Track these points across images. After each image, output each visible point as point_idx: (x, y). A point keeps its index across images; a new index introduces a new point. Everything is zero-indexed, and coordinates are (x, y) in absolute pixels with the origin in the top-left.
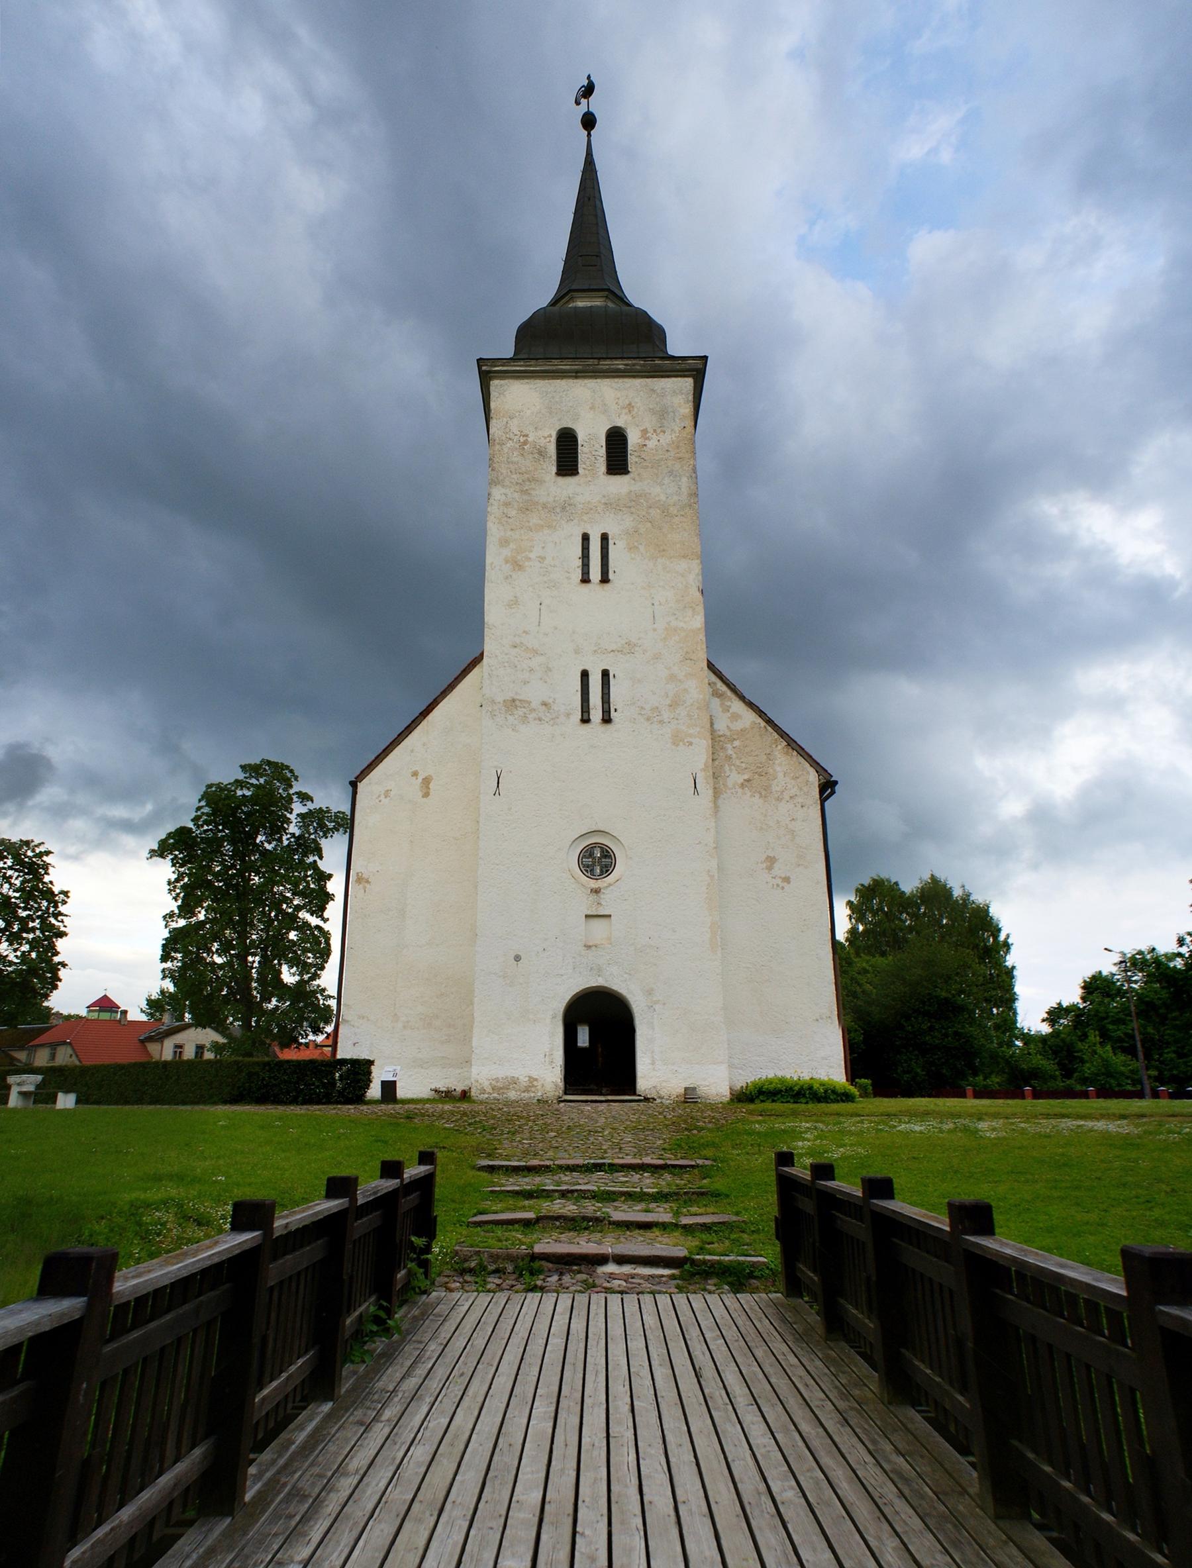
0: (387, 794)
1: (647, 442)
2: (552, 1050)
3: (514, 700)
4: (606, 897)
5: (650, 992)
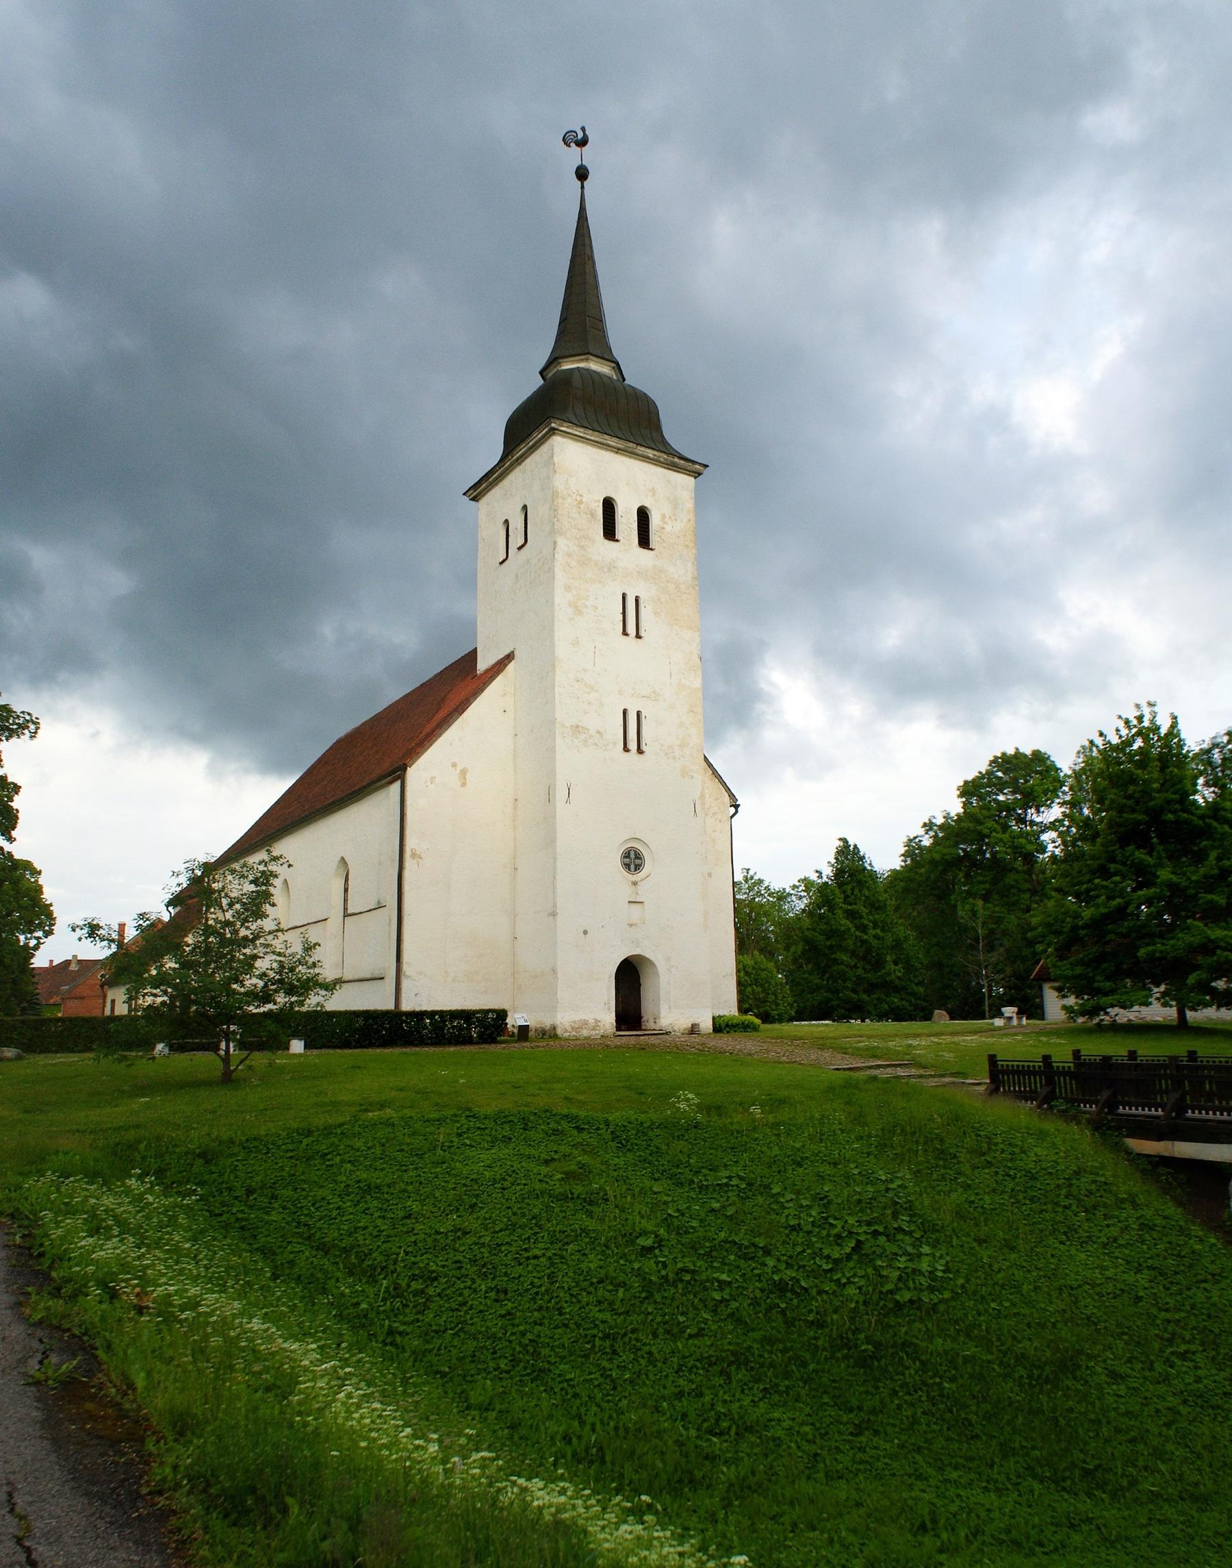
0: (432, 779)
4: (642, 887)
5: (668, 959)
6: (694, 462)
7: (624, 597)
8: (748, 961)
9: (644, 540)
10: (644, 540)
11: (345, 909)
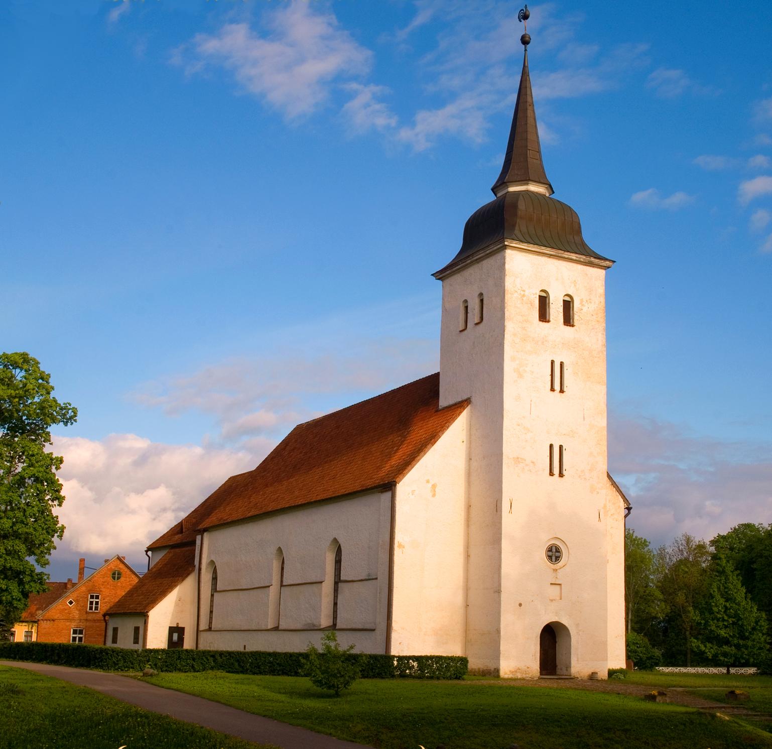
0: (413, 491)
1: (583, 308)
2: (535, 652)
3: (518, 458)
4: (560, 573)
5: (577, 625)
6: (606, 259)
7: (553, 362)
8: (695, 665)
9: (568, 320)
10: (568, 320)
11: (282, 581)
